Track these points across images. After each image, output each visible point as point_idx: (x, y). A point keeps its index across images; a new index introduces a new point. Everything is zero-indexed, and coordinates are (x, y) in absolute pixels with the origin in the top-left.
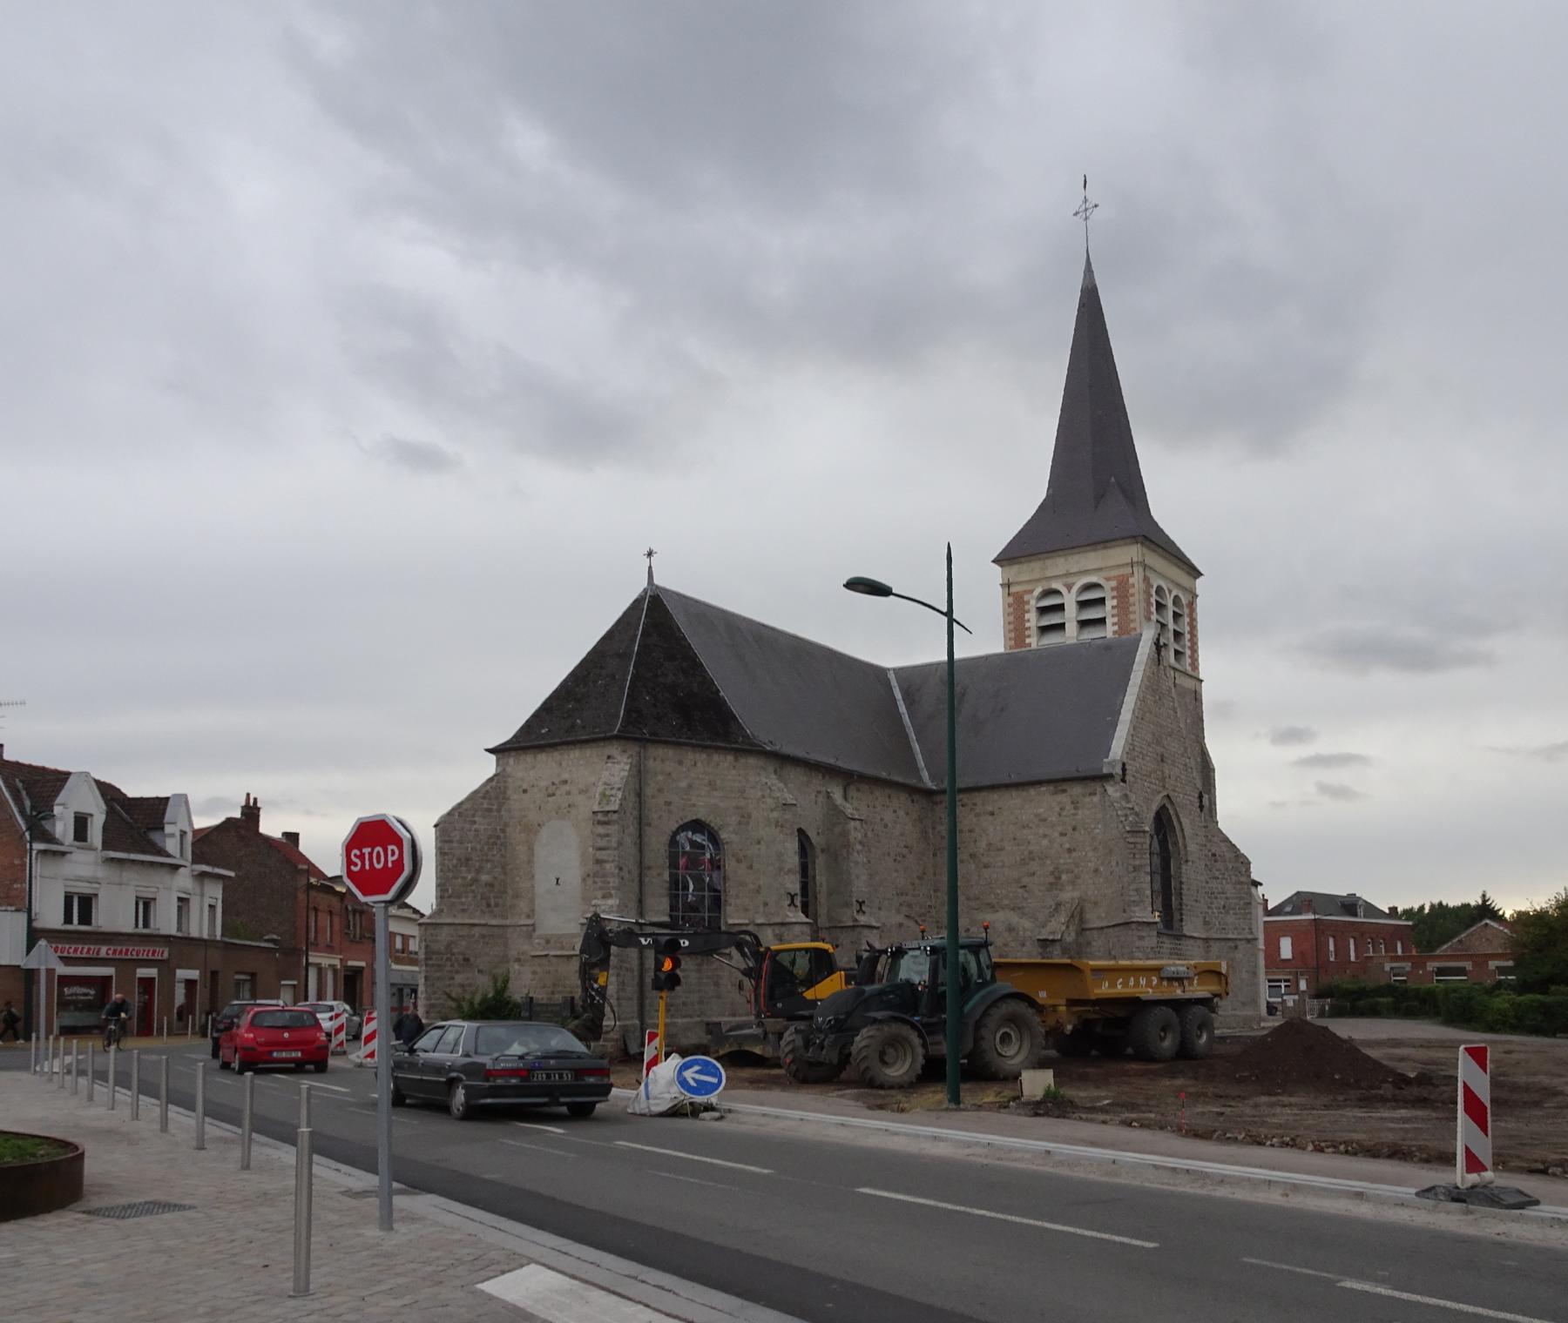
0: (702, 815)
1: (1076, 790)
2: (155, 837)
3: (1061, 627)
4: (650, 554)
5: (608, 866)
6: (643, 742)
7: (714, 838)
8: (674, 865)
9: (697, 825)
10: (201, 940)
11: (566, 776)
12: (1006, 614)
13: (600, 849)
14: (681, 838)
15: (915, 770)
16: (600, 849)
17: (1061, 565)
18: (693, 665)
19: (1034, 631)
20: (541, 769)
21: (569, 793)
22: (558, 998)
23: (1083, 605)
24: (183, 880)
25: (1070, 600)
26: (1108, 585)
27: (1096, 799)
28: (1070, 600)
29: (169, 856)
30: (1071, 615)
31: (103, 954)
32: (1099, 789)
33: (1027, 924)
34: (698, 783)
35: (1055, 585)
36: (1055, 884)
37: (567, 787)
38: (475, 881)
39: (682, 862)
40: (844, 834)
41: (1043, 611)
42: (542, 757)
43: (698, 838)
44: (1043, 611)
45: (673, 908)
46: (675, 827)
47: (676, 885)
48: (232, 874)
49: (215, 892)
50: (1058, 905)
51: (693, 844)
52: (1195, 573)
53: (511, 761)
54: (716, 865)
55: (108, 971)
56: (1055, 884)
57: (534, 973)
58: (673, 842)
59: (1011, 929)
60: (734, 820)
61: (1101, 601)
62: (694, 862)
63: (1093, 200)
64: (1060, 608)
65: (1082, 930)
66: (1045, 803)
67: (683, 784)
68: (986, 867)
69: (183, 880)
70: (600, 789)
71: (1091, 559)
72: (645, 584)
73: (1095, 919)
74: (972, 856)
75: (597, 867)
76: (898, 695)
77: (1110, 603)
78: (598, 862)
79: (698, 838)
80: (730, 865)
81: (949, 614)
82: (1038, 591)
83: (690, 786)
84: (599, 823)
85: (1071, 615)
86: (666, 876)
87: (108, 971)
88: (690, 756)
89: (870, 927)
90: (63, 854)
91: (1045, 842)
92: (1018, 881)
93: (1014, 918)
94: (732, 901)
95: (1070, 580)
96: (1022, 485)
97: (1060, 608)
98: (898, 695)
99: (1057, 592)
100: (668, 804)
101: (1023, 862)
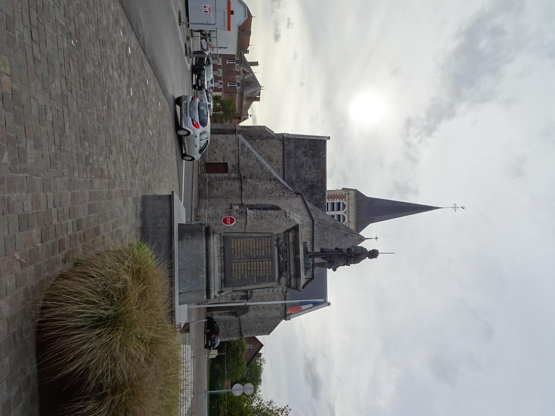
17: (352, 210)
19: (333, 201)
25: (341, 213)
28: (341, 213)
35: (346, 209)
82: (345, 203)
85: (336, 213)
95: (347, 213)
99: (344, 208)
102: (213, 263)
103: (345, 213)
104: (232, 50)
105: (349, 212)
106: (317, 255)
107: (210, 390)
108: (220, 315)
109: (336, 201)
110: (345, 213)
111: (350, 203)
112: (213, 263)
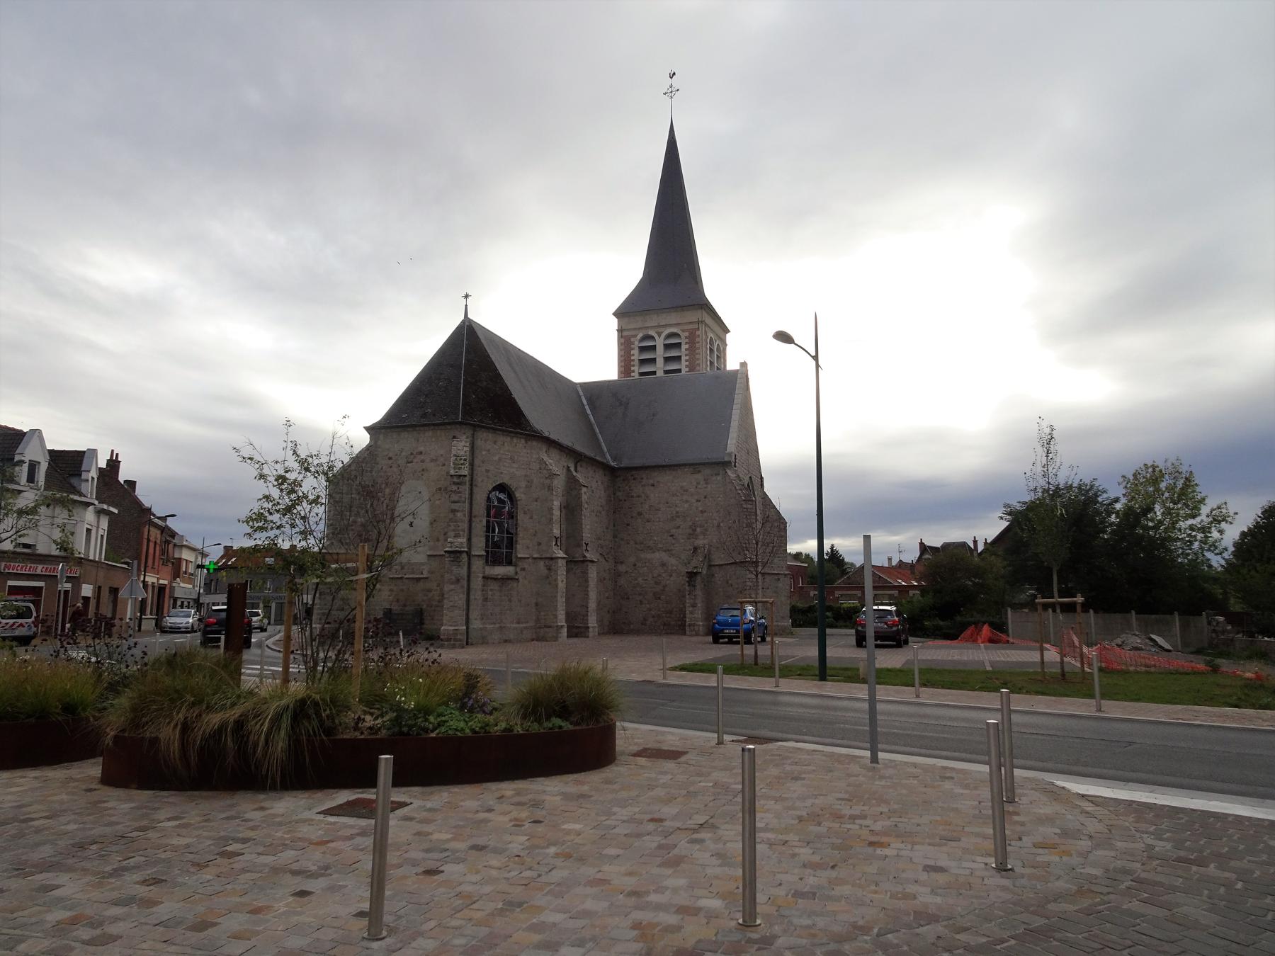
0: (506, 480)
1: (707, 471)
2: (74, 481)
3: (654, 360)
4: (466, 296)
5: (459, 514)
6: (474, 427)
7: (511, 497)
8: (488, 515)
9: (502, 488)
10: (94, 561)
11: (422, 449)
12: (620, 350)
13: (454, 502)
14: (493, 495)
15: (603, 455)
16: (454, 502)
17: (654, 320)
18: (497, 377)
19: (636, 362)
20: (405, 443)
21: (423, 461)
22: (409, 609)
23: (667, 347)
24: (90, 515)
25: (660, 343)
26: (683, 335)
27: (719, 478)
28: (660, 343)
29: (81, 495)
30: (660, 353)
31: (39, 572)
32: (721, 472)
33: (673, 561)
34: (505, 459)
35: (652, 333)
36: (693, 534)
37: (422, 457)
38: (355, 522)
39: (492, 513)
40: (579, 496)
41: (642, 349)
42: (405, 435)
43: (502, 496)
44: (642, 349)
45: (487, 546)
46: (490, 488)
47: (489, 528)
48: (116, 511)
49: (105, 523)
50: (695, 549)
51: (500, 500)
52: (726, 331)
53: (381, 437)
54: (512, 516)
55: (41, 584)
56: (693, 534)
57: (391, 590)
58: (489, 499)
59: (663, 565)
60: (523, 484)
61: (678, 345)
62: (499, 513)
63: (676, 86)
64: (653, 348)
65: (710, 566)
66: (687, 480)
67: (496, 458)
68: (648, 521)
69: (90, 515)
70: (453, 459)
71: (673, 318)
72: (462, 318)
73: (718, 559)
74: (640, 514)
75: (451, 516)
76: (585, 402)
77: (684, 347)
78: (454, 511)
79: (502, 496)
80: (520, 516)
81: (816, 358)
82: (640, 335)
83: (500, 459)
84: (455, 483)
85: (660, 353)
86: (484, 523)
87: (41, 584)
88: (501, 439)
89: (592, 562)
90: (20, 492)
91: (686, 506)
92: (668, 532)
93: (664, 556)
94: (520, 541)
95: (660, 330)
96: (627, 266)
97: (653, 348)
98: (585, 402)
99: (652, 338)
100: (487, 471)
101: (672, 519)
102: (852, 714)
103: (659, 334)
104: (109, 615)
105: (659, 326)
106: (286, 667)
107: (921, 671)
108: (694, 606)
109: (636, 355)
110: (659, 334)
111: (639, 325)
112: (852, 714)
